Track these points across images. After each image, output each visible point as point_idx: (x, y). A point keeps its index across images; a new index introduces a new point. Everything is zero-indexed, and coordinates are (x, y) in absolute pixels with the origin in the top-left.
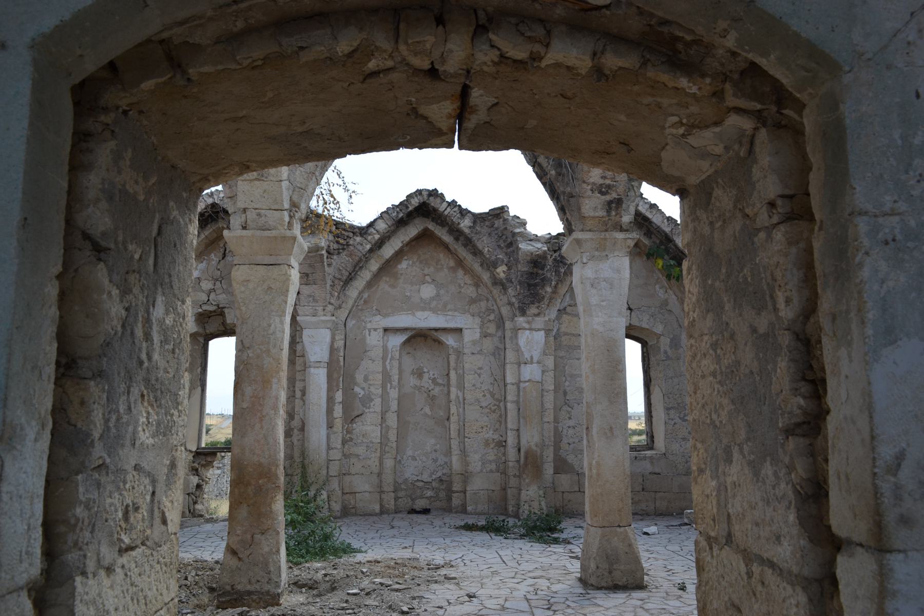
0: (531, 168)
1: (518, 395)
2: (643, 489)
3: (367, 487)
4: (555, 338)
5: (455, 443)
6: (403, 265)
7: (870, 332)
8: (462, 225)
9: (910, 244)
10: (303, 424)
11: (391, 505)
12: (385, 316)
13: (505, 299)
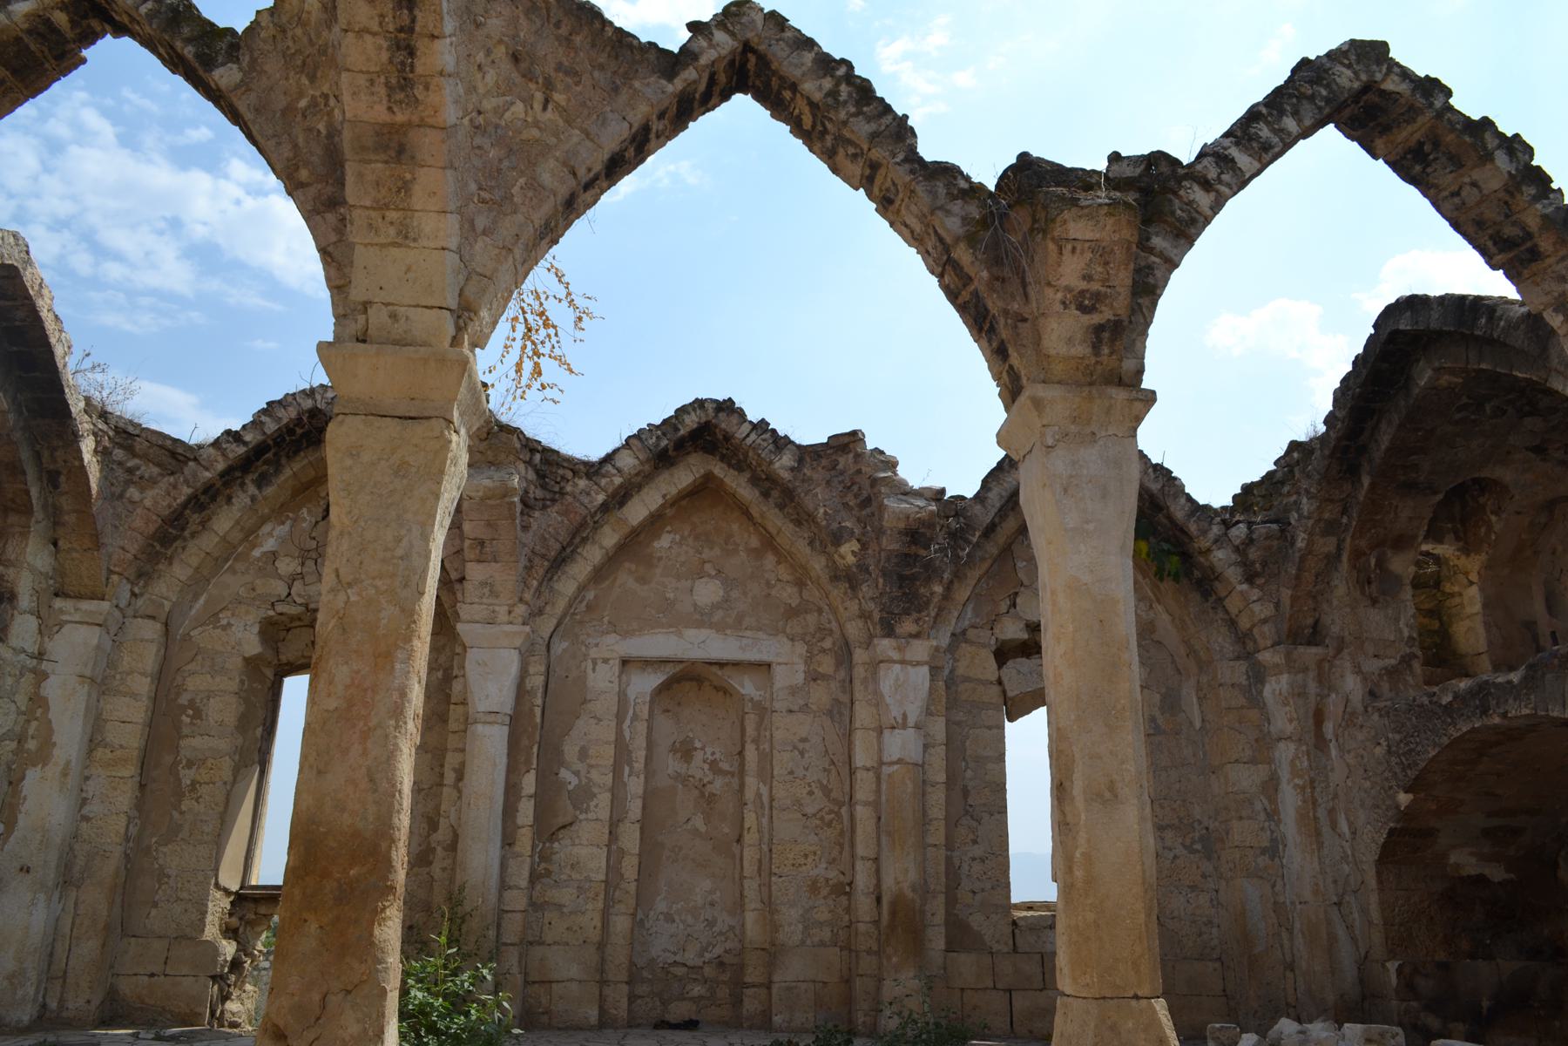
0: (934, 280)
1: (878, 791)
3: (574, 971)
5: (751, 887)
6: (664, 542)
8: (777, 465)
10: (456, 837)
11: (621, 1009)
12: (626, 634)
13: (854, 607)
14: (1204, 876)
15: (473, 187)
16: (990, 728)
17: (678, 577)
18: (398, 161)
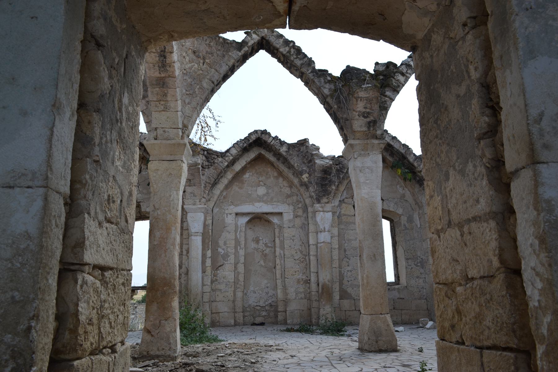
0: (322, 106)
1: (317, 251)
2: (394, 308)
3: (226, 309)
4: (338, 217)
5: (279, 282)
6: (247, 175)
7: (521, 53)
8: (281, 150)
9: (540, 10)
11: (241, 320)
12: (236, 205)
13: (308, 194)
14: (421, 273)
15: (184, 91)
16: (352, 230)
17: (252, 187)
18: (163, 88)
